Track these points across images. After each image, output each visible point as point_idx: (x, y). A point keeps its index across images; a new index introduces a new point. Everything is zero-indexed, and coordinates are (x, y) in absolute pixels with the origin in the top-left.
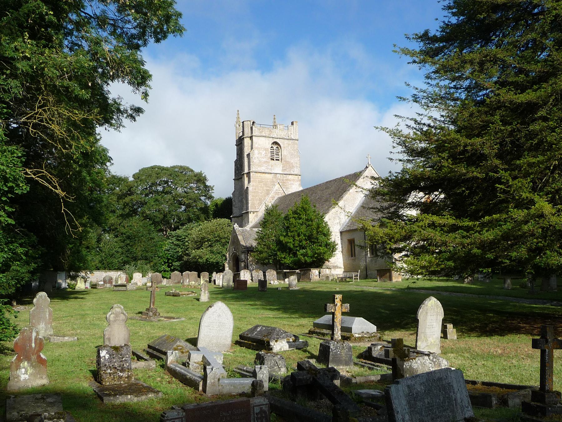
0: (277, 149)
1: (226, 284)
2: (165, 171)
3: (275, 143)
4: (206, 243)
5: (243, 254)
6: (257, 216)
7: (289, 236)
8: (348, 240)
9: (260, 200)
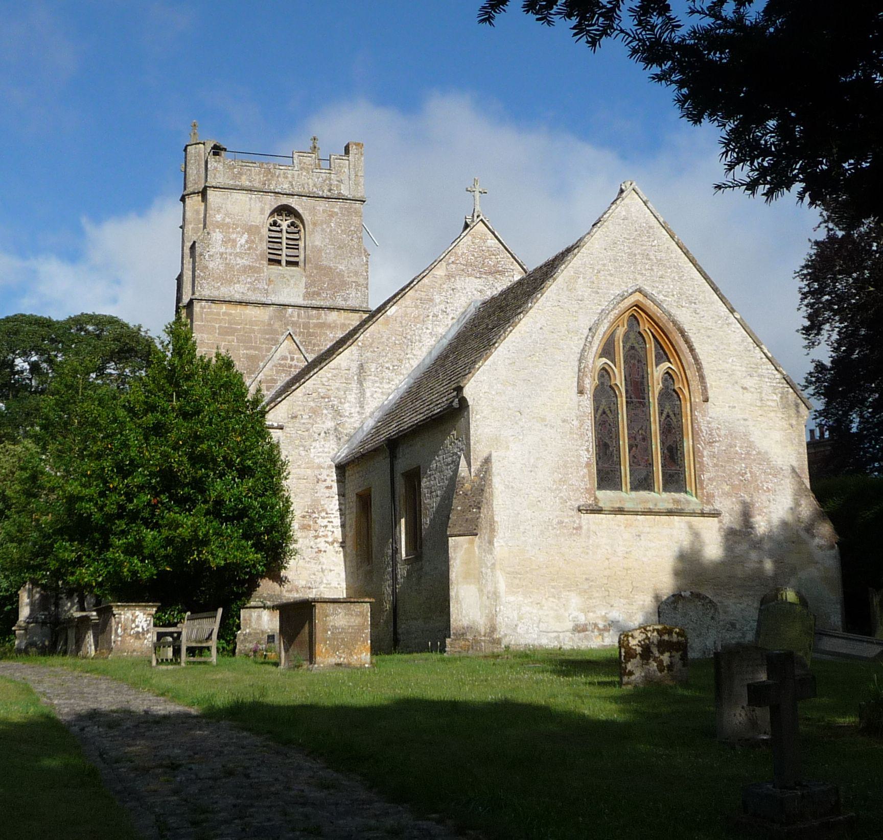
0: (292, 229)
3: (285, 210)
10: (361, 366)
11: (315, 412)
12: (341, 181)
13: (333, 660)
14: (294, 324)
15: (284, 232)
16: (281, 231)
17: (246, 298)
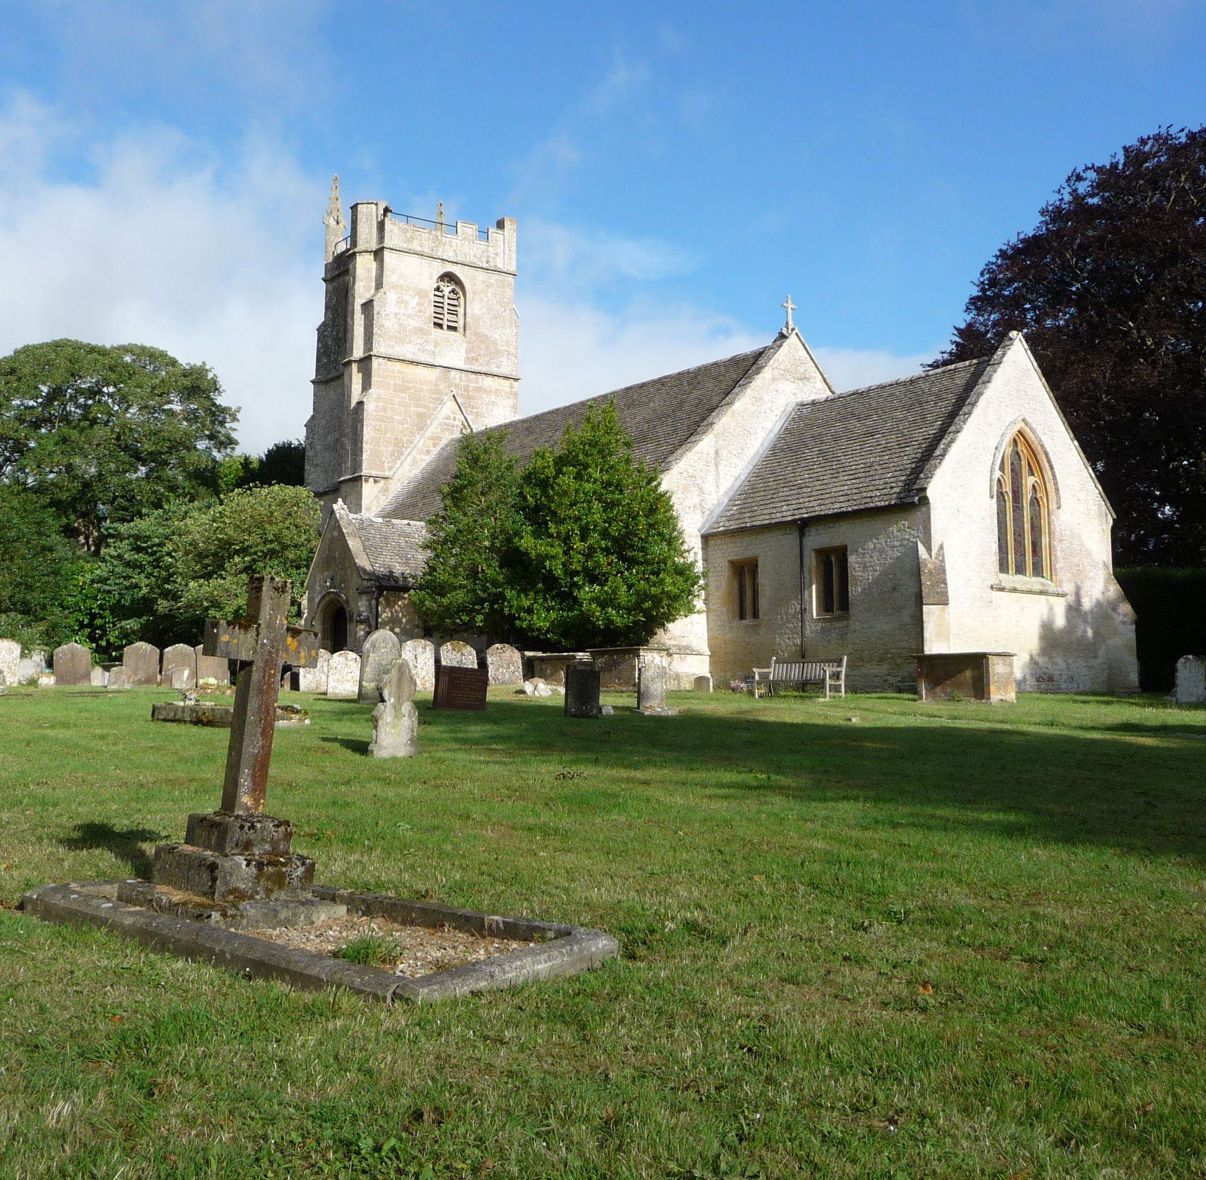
0: (452, 295)
1: (373, 685)
2: (95, 355)
3: (449, 277)
4: (237, 559)
5: (364, 597)
6: (386, 490)
7: (551, 536)
8: (732, 563)
9: (396, 445)
10: (717, 452)
12: (497, 254)
13: (1000, 697)
14: (456, 386)
15: (446, 298)
16: (443, 297)
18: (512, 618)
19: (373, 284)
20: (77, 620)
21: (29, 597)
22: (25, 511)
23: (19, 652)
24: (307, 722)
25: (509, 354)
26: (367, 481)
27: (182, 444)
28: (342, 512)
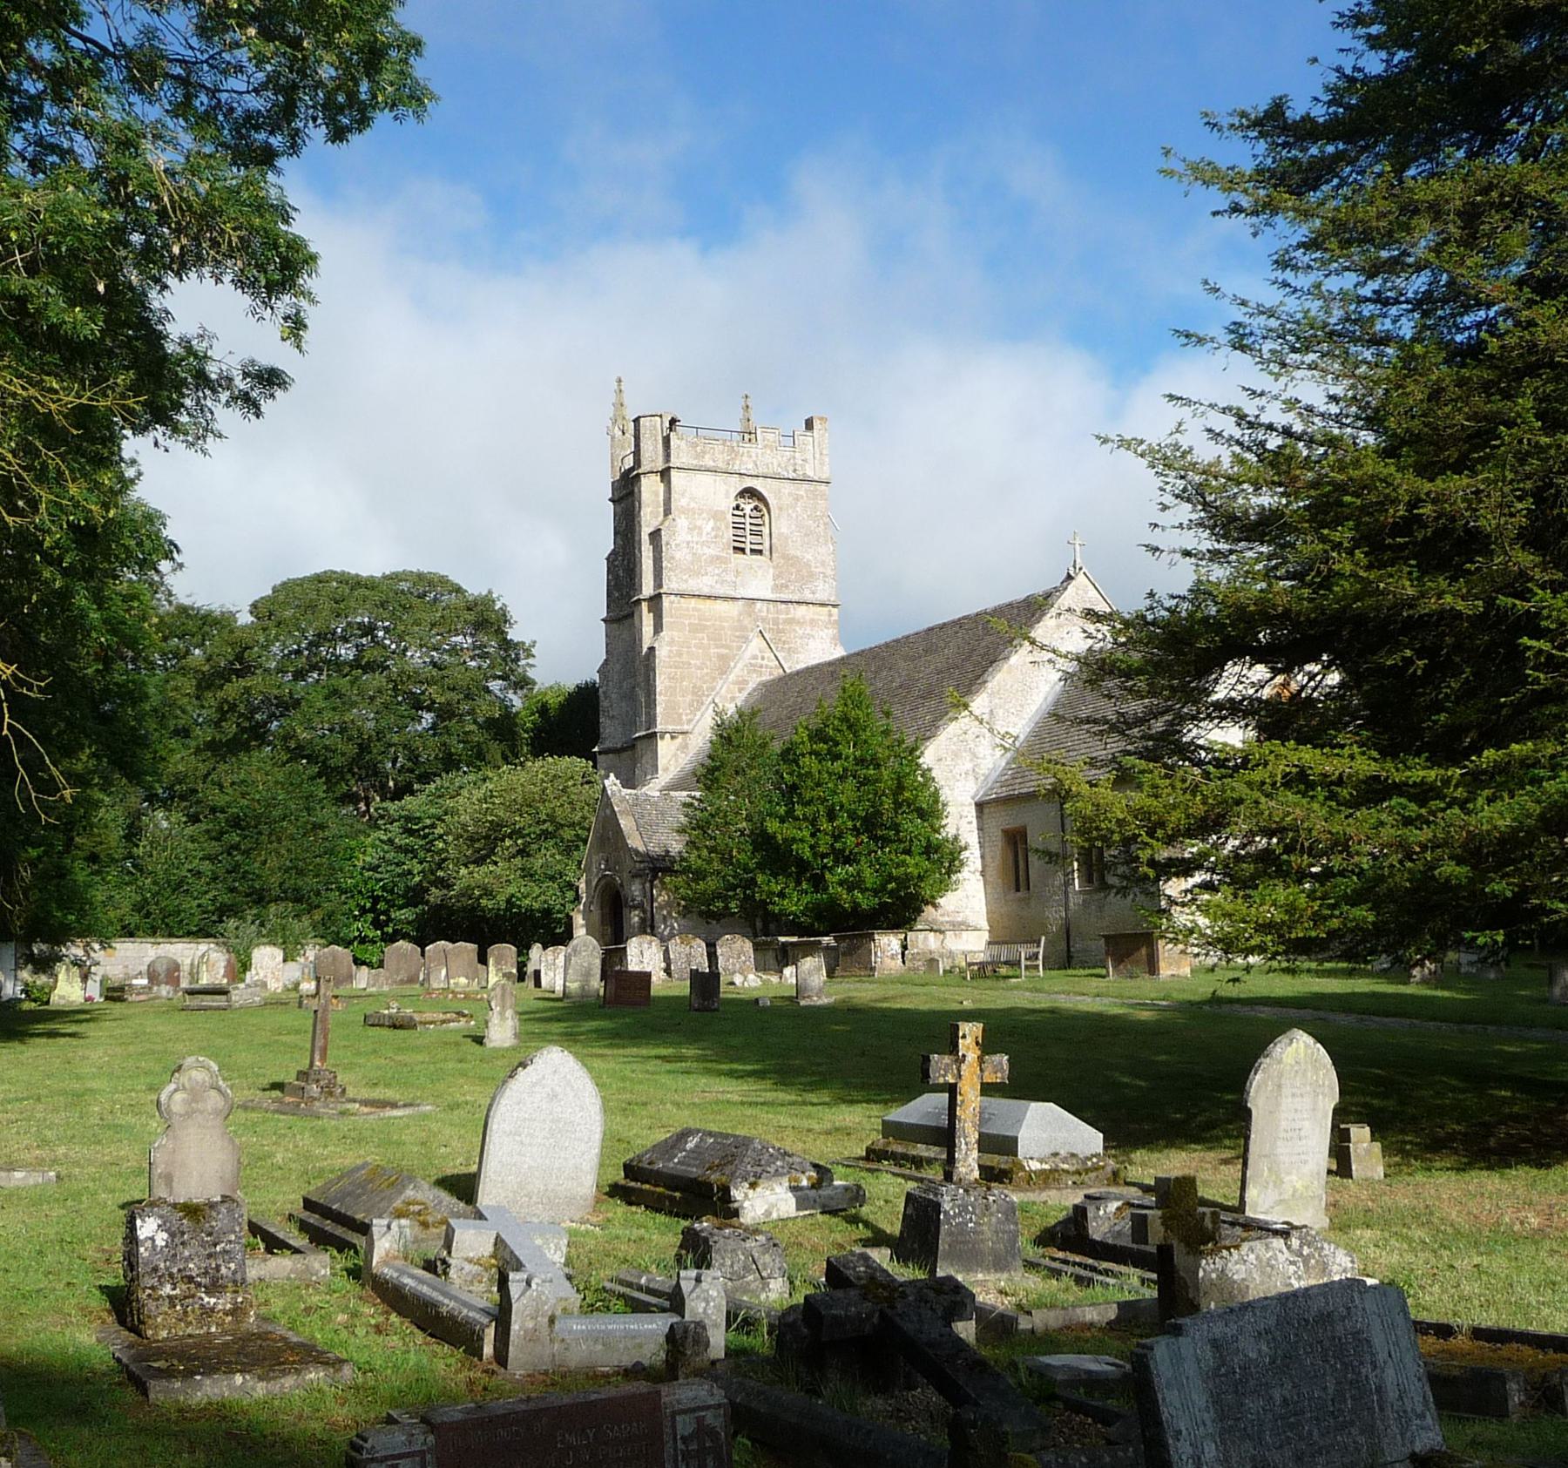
0: (755, 513)
3: (750, 493)
4: (508, 843)
5: (638, 881)
6: (684, 747)
7: (797, 819)
8: (1005, 832)
9: (694, 693)
11: (956, 755)
13: (1170, 973)
14: (763, 620)
16: (744, 516)
17: (714, 592)
18: (764, 903)
19: (662, 509)
20: (358, 905)
21: (300, 883)
22: (292, 784)
23: (281, 958)
24: (473, 1023)
25: (825, 576)
26: (662, 738)
27: (474, 690)
28: (614, 788)
